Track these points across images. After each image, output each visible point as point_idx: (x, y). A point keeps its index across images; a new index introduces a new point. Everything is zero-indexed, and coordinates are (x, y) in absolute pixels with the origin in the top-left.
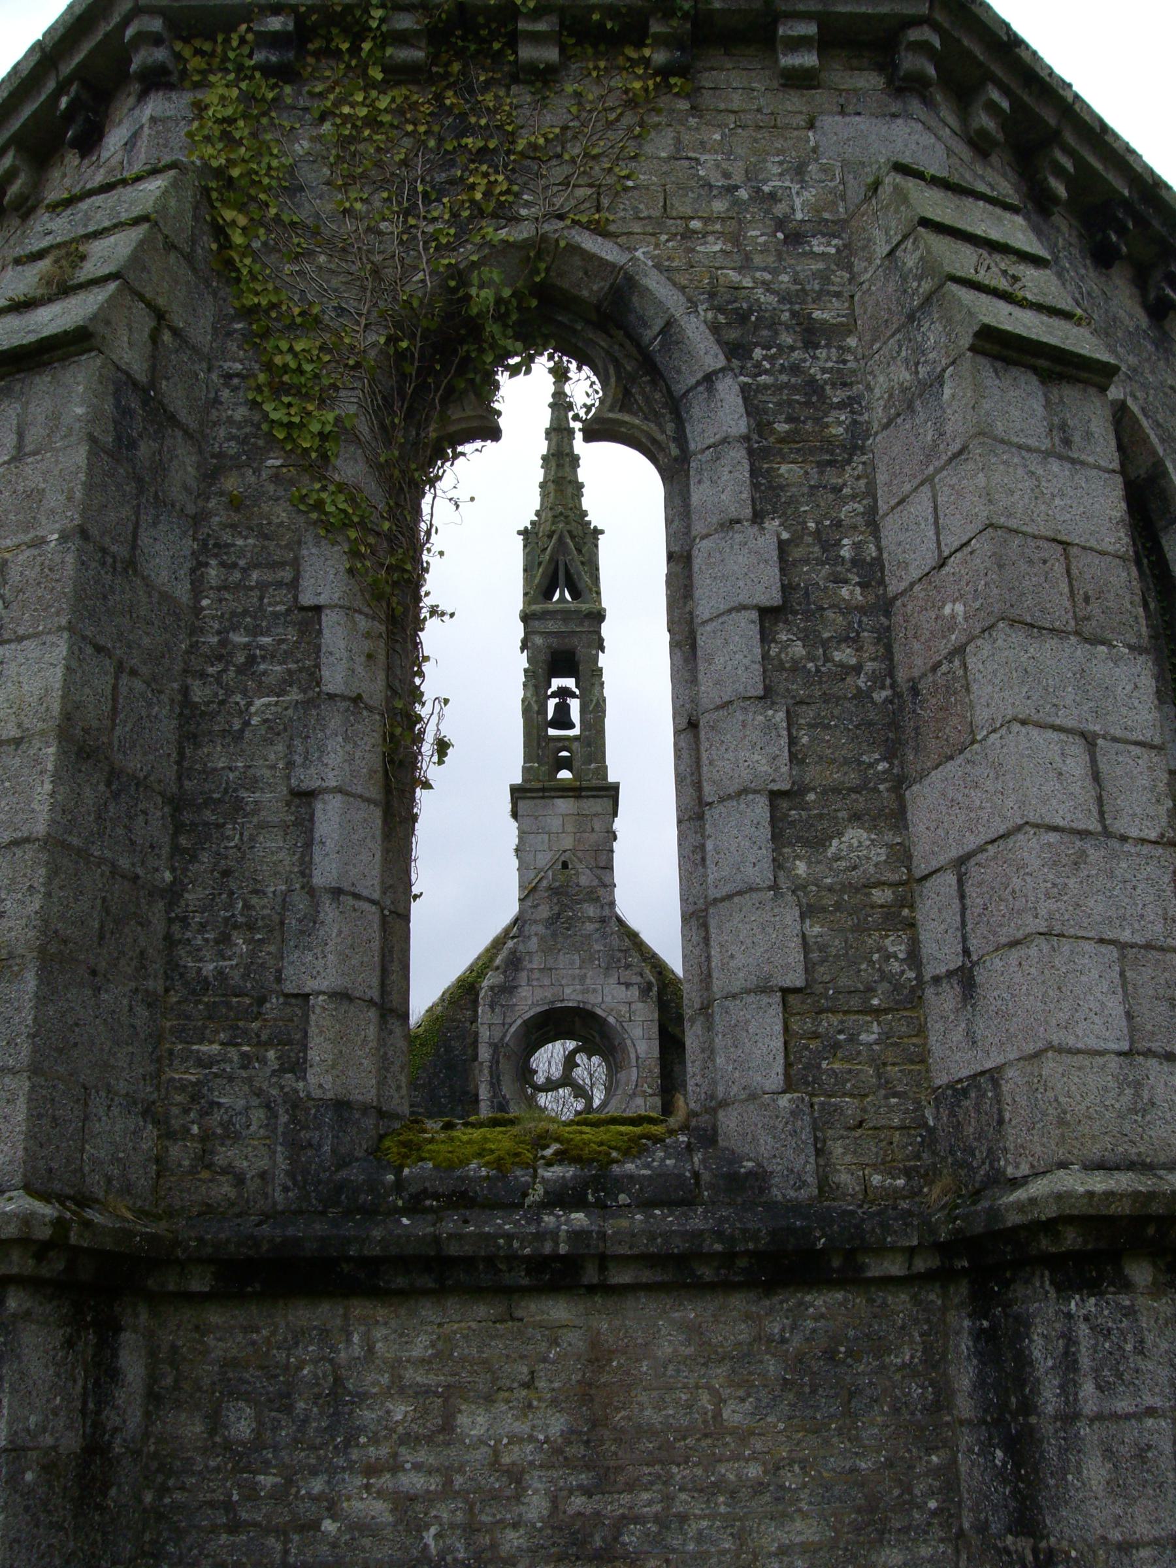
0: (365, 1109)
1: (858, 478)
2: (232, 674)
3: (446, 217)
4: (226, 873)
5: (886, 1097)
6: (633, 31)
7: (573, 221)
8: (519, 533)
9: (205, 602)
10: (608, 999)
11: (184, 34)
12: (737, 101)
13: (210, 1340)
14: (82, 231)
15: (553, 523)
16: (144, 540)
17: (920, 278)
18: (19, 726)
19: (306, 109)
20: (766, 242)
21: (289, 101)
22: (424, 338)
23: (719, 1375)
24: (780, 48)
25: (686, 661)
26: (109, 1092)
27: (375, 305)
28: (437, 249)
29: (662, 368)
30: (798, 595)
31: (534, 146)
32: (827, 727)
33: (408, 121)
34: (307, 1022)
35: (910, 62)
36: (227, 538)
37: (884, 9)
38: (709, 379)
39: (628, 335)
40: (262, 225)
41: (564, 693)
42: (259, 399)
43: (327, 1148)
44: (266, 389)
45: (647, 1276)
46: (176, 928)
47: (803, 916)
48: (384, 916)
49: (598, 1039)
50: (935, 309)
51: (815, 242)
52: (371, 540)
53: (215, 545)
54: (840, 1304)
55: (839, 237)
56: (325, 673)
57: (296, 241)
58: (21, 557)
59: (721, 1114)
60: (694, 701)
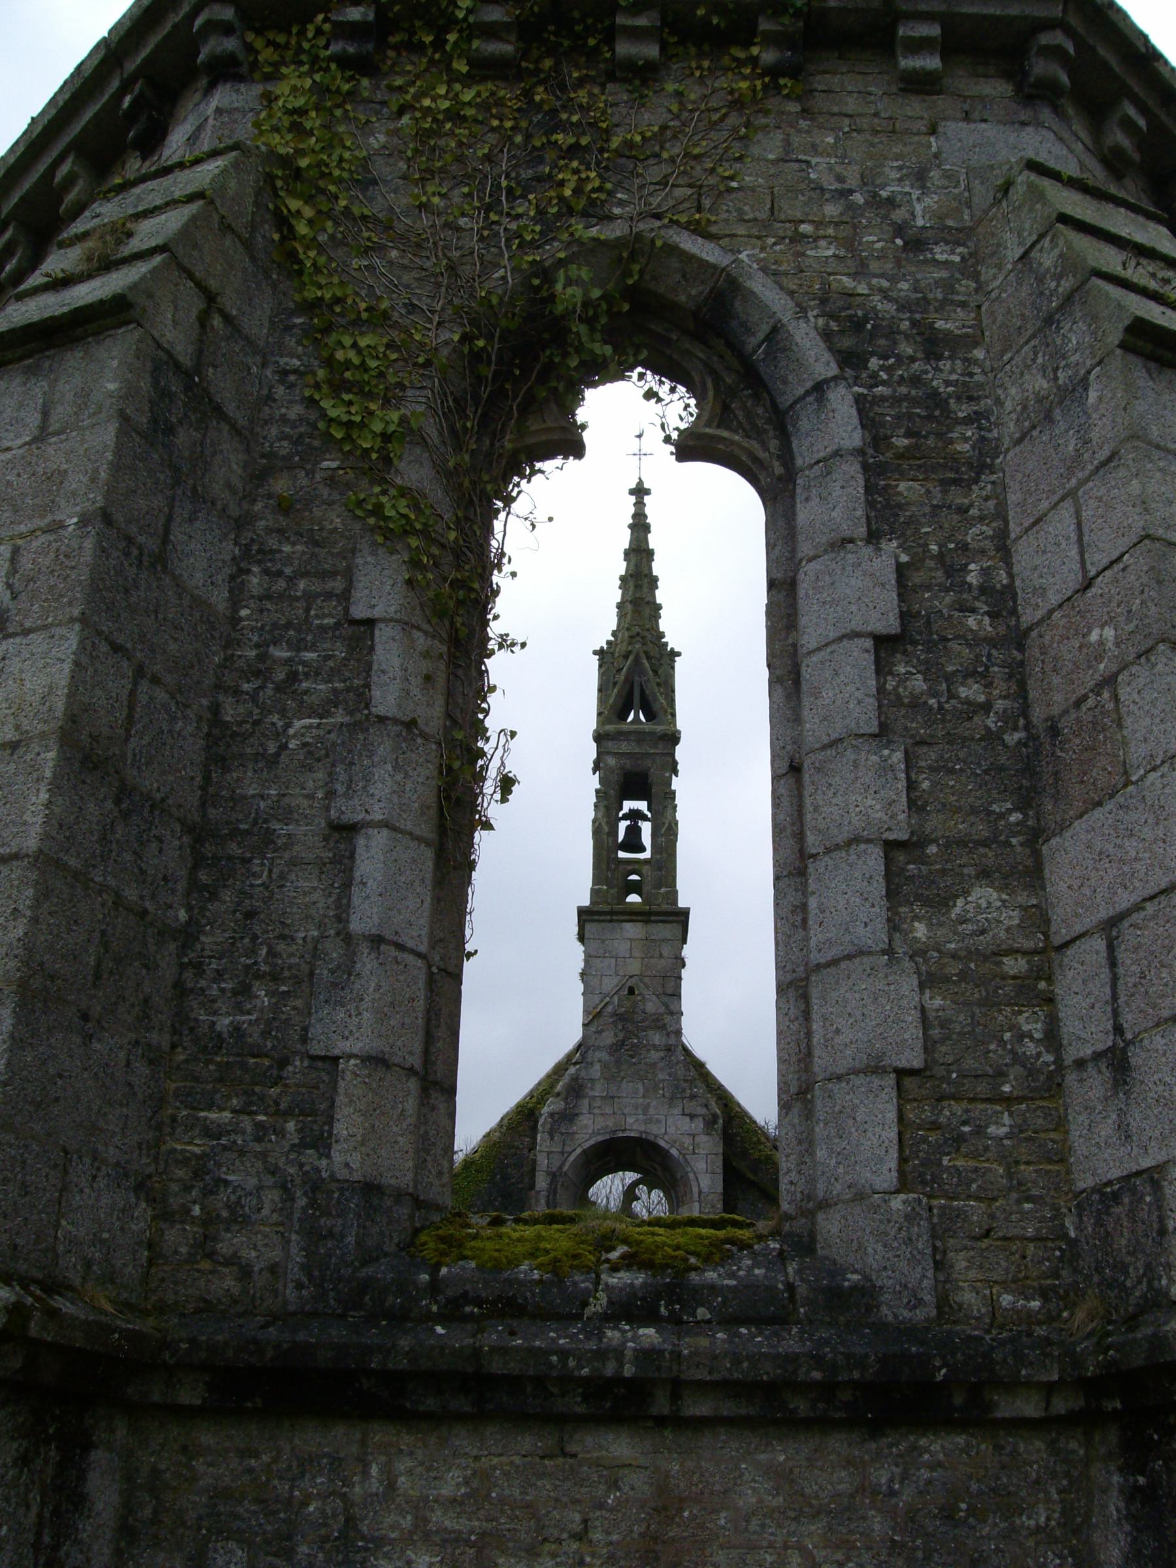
0: (399, 1195)
1: (987, 499)
2: (269, 691)
3: (532, 213)
4: (250, 915)
5: (1019, 1202)
6: (742, 31)
7: (671, 220)
8: (595, 653)
9: (244, 613)
10: (672, 1130)
11: (257, 25)
12: (852, 105)
13: (199, 1464)
14: (131, 211)
15: (630, 644)
16: (177, 534)
17: (1059, 278)
18: (17, 727)
19: (383, 103)
20: (882, 249)
21: (366, 94)
22: (502, 339)
23: (813, 1532)
24: (899, 50)
25: (788, 697)
26: (95, 1159)
27: (451, 302)
28: (520, 246)
29: (766, 378)
30: (919, 624)
31: (629, 144)
32: (952, 771)
33: (493, 116)
34: (335, 1089)
35: (1040, 68)
36: (272, 542)
37: (1014, 11)
38: (819, 388)
39: (729, 345)
40: (330, 218)
41: (635, 815)
42: (317, 397)
43: (351, 1239)
44: (325, 387)
45: (728, 1408)
46: (188, 974)
47: (922, 986)
48: (432, 974)
49: (659, 1172)
50: (1077, 307)
51: (937, 249)
52: (435, 551)
53: (259, 551)
54: (962, 1451)
55: (964, 245)
56: (376, 693)
57: (366, 234)
58: (34, 544)
59: (820, 1216)
60: (797, 742)
